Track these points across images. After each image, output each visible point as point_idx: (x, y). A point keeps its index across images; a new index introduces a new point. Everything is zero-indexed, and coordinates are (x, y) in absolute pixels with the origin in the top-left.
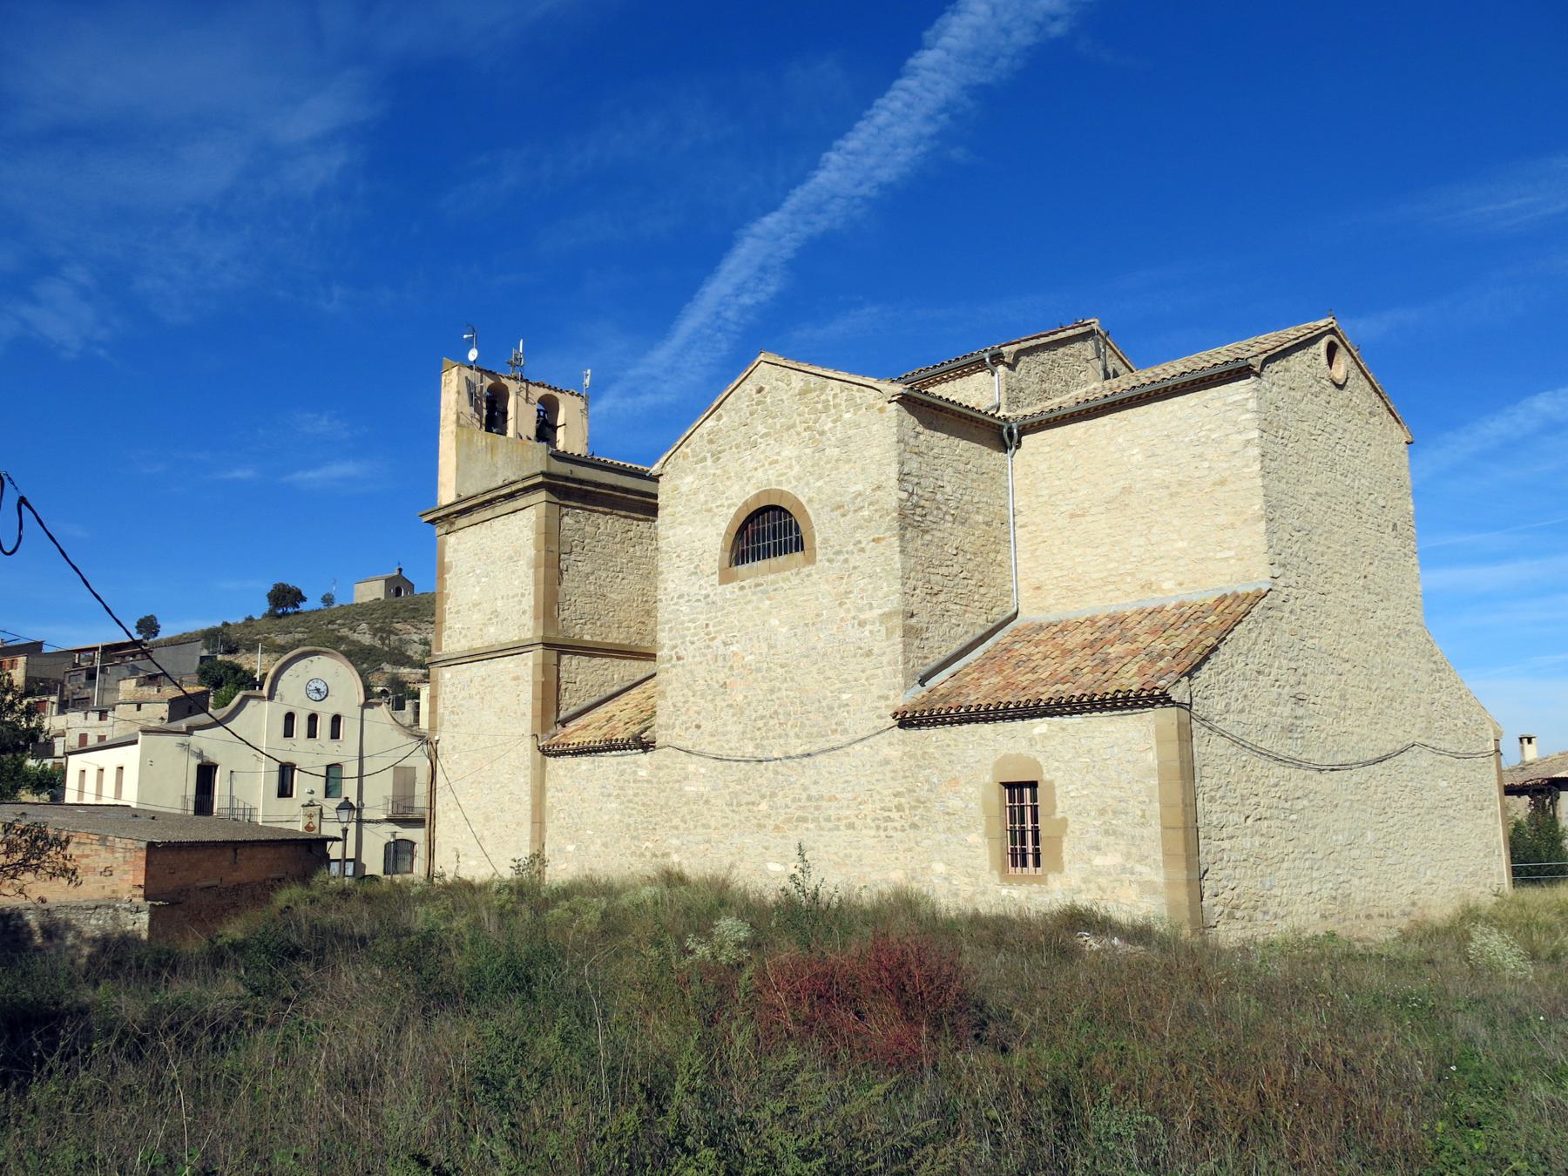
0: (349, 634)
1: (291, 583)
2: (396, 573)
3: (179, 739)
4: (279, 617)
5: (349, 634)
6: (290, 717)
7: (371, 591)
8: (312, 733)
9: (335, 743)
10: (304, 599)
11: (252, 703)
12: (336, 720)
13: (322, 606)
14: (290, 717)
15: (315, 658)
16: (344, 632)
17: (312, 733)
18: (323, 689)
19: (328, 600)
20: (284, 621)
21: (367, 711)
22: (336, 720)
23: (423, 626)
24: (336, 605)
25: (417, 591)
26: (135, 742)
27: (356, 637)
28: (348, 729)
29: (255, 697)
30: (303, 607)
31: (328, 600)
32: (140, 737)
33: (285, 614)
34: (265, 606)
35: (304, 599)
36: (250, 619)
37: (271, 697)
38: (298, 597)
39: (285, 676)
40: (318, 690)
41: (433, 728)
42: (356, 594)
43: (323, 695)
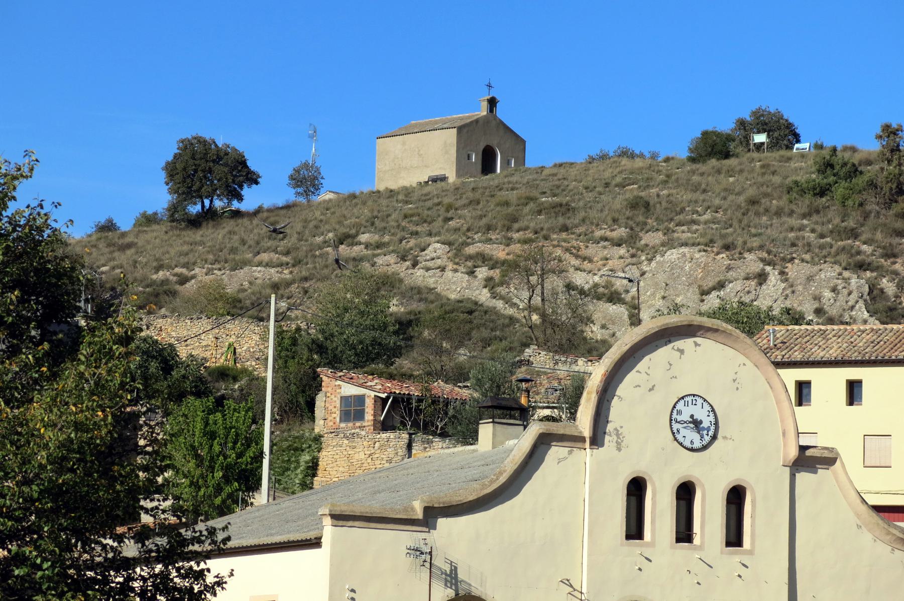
0: (401, 269)
1: (223, 138)
2: (483, 111)
3: (407, 537)
4: (195, 222)
5: (401, 269)
6: (637, 488)
7: (421, 158)
8: (684, 534)
9: (734, 557)
10: (253, 179)
11: (556, 452)
12: (736, 497)
13: (288, 195)
14: (637, 488)
15: (686, 344)
16: (387, 263)
17: (684, 534)
18: (702, 414)
19: (306, 180)
20: (209, 234)
21: (803, 478)
22: (736, 497)
23: (592, 250)
24: (325, 196)
25: (532, 160)
26: (315, 543)
27: (419, 277)
28: (762, 518)
29: (562, 438)
30: (251, 198)
31: (306, 180)
32: (328, 531)
33: (210, 215)
34: (159, 198)
35: (253, 179)
36: (108, 227)
37: (597, 440)
38: (237, 173)
39: (625, 388)
40: (696, 424)
41: (702, 542)
42: (382, 165)
43: (706, 434)
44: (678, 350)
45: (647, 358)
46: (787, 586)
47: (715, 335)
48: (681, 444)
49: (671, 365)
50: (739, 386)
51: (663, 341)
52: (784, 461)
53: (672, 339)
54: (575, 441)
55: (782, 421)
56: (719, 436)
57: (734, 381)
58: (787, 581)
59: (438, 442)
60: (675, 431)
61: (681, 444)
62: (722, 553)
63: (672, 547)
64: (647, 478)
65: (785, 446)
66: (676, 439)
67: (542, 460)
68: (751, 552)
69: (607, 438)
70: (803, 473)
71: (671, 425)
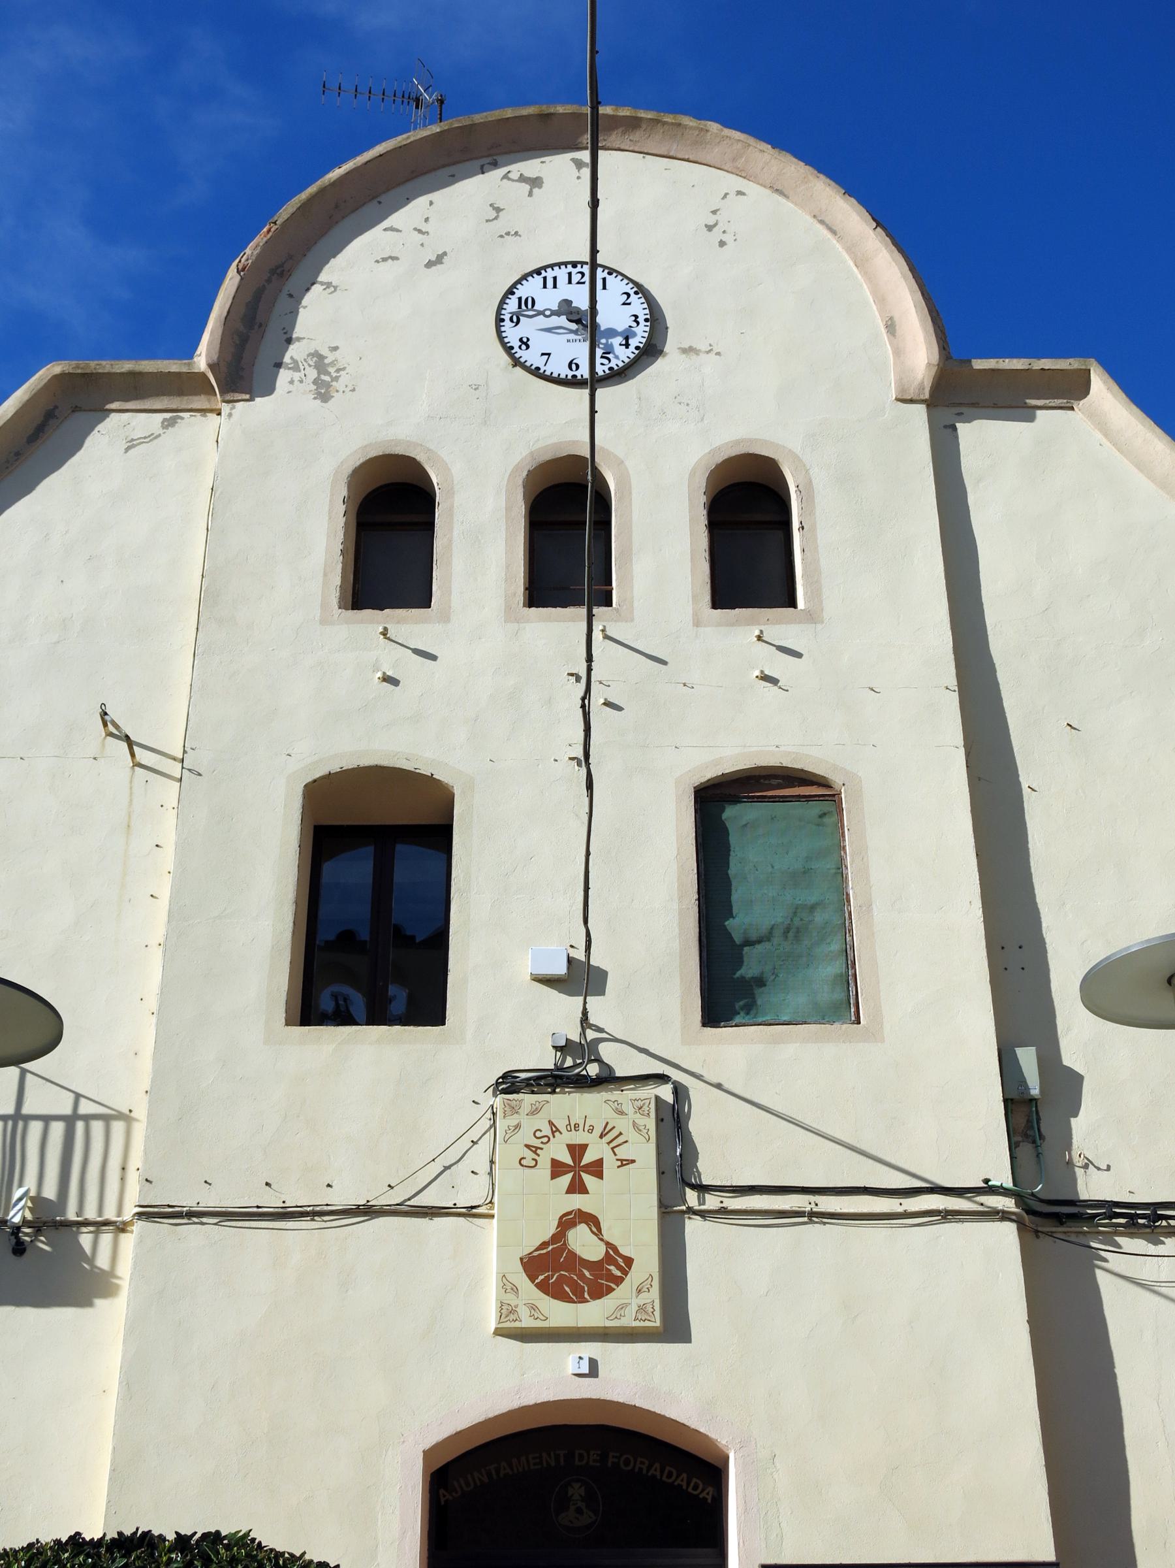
21: (982, 440)
44: (522, 179)
45: (422, 202)
46: (954, 698)
47: (637, 135)
48: (536, 372)
49: (1109, 1168)
50: (725, 238)
51: (477, 163)
52: (901, 388)
53: (499, 159)
54: (181, 393)
55: (881, 300)
56: (671, 345)
57: (710, 228)
58: (953, 682)
59: (1000, 1208)
60: (516, 344)
61: (536, 372)
62: (697, 623)
63: (509, 616)
64: (420, 457)
65: (898, 352)
66: (517, 362)
67: (77, 446)
68: (812, 617)
69: (284, 376)
70: (977, 424)
71: (499, 333)
